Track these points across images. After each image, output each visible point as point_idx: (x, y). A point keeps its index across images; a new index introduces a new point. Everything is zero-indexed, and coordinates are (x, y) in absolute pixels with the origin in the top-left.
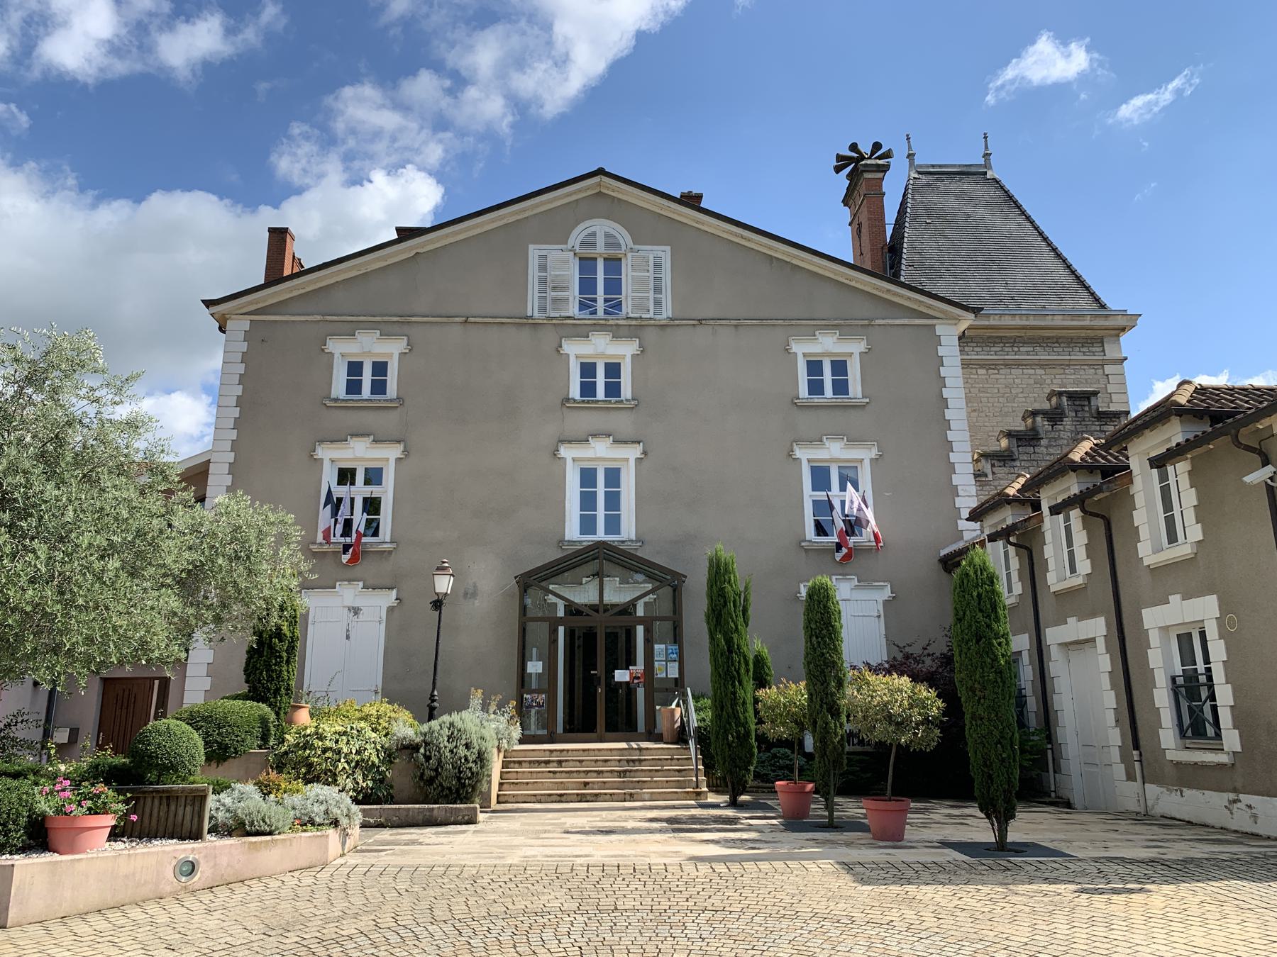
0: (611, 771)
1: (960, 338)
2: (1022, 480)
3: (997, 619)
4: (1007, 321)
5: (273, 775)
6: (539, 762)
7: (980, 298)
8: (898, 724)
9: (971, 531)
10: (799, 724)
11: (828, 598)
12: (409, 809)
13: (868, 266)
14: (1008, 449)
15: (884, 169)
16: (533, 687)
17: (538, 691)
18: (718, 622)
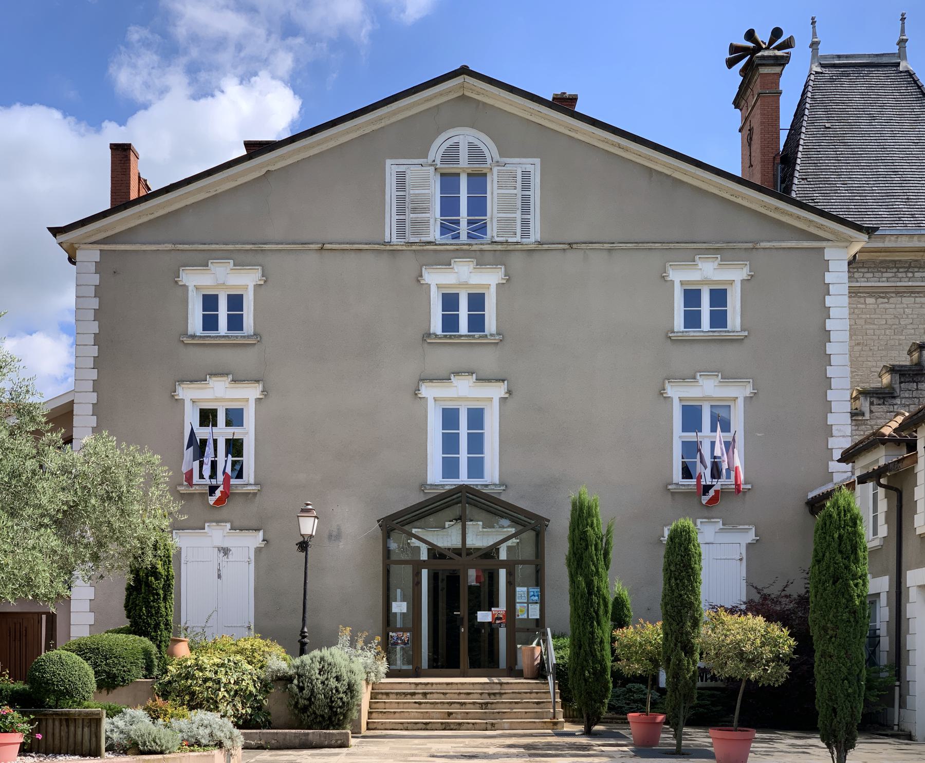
0: (474, 703)
1: (850, 263)
2: (900, 419)
3: (857, 561)
4: (904, 243)
5: (160, 701)
6: (405, 694)
7: (877, 216)
8: (750, 661)
9: (841, 472)
10: (654, 662)
11: (689, 540)
12: (286, 733)
13: (757, 180)
14: (890, 386)
15: (782, 62)
16: (398, 626)
17: (404, 630)
18: (579, 565)
